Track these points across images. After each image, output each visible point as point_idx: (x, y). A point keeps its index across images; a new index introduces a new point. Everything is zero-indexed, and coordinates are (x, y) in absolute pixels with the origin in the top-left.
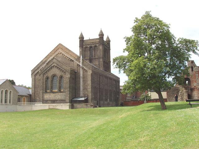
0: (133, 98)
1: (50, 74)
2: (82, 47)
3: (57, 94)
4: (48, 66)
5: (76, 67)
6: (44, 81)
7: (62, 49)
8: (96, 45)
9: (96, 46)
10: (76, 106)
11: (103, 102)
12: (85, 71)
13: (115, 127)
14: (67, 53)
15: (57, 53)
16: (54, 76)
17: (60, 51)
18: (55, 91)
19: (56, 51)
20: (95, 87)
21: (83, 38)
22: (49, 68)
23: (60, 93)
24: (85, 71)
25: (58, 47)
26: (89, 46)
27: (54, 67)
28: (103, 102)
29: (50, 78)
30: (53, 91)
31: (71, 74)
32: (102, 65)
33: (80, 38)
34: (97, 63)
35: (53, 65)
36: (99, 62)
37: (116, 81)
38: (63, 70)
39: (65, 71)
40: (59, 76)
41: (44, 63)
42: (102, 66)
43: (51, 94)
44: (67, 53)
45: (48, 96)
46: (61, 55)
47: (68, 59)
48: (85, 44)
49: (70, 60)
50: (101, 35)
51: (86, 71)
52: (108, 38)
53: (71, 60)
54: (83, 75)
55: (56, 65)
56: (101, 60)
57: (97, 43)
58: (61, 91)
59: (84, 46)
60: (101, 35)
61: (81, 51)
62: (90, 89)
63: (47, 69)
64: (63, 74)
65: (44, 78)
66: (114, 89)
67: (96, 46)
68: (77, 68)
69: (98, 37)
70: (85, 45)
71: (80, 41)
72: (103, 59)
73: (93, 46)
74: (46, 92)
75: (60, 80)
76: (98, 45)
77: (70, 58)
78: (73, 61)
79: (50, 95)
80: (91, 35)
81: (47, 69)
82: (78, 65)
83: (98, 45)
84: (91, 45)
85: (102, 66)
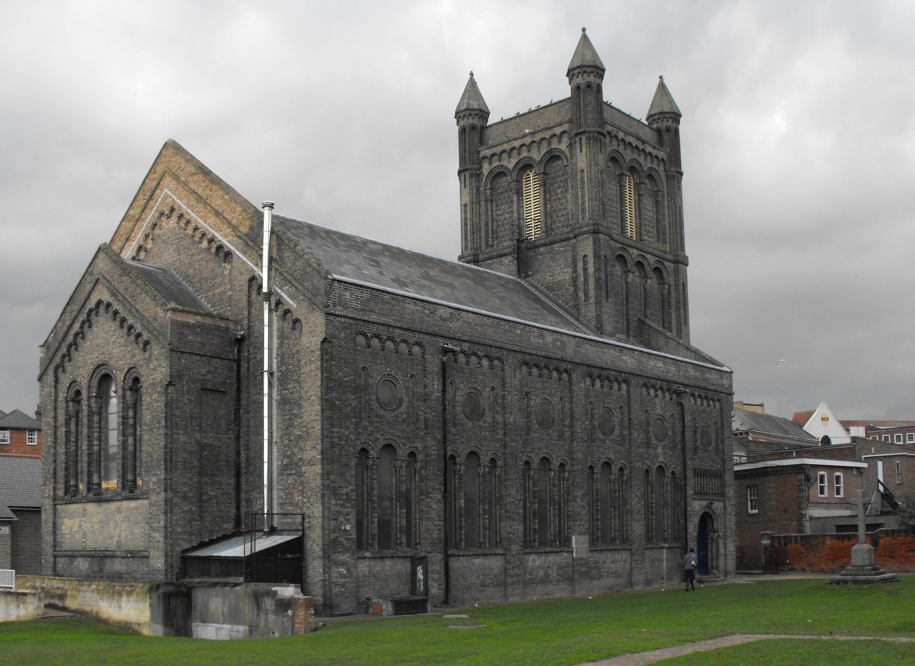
2: (478, 175)
4: (76, 307)
6: (61, 418)
8: (555, 145)
9: (553, 157)
10: (206, 606)
11: (721, 504)
15: (151, 216)
21: (484, 114)
23: (125, 504)
24: (288, 325)
25: (160, 169)
27: (102, 309)
28: (721, 504)
31: (175, 351)
33: (460, 115)
34: (562, 274)
35: (92, 303)
39: (146, 336)
42: (592, 293)
44: (200, 199)
48: (488, 153)
50: (587, 72)
53: (220, 248)
54: (282, 359)
59: (486, 168)
60: (587, 72)
61: (467, 199)
62: (318, 468)
67: (553, 157)
69: (564, 90)
72: (596, 242)
73: (536, 155)
76: (563, 146)
78: (228, 255)
80: (524, 82)
83: (563, 146)
84: (525, 154)
85: (592, 293)
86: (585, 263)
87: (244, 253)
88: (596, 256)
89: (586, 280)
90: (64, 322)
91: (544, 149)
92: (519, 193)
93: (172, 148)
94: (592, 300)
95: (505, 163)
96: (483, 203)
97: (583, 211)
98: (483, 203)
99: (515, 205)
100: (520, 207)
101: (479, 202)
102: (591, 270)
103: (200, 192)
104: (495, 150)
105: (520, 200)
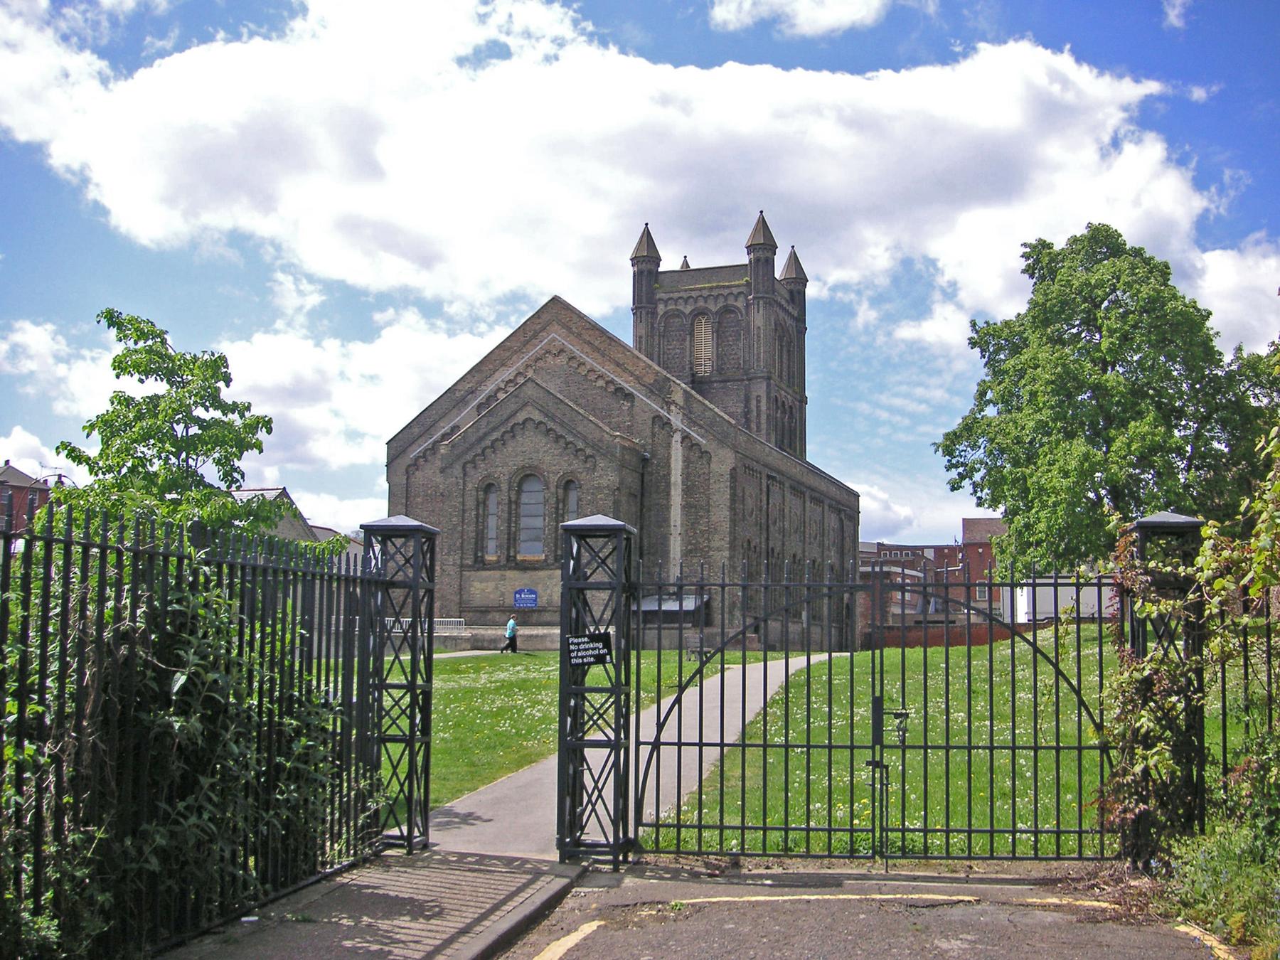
0: (925, 611)
1: (504, 465)
2: (653, 313)
3: (542, 574)
5: (648, 433)
6: (470, 503)
7: (569, 329)
8: (731, 301)
9: (727, 310)
12: (694, 455)
13: (1122, 644)
14: (597, 350)
16: (527, 475)
17: (554, 340)
18: (529, 557)
19: (535, 336)
20: (749, 542)
22: (496, 435)
24: (694, 455)
26: (688, 309)
27: (529, 425)
29: (504, 487)
30: (519, 557)
32: (764, 417)
33: (635, 260)
35: (521, 417)
36: (747, 400)
37: (840, 511)
38: (580, 445)
39: (589, 451)
40: (554, 479)
41: (463, 402)
42: (764, 426)
43: (509, 574)
45: (491, 585)
46: (562, 360)
47: (601, 383)
49: (611, 388)
50: (763, 245)
51: (705, 454)
52: (794, 259)
53: (620, 390)
54: (686, 476)
55: (537, 416)
56: (760, 389)
57: (735, 291)
58: (483, 561)
59: (661, 309)
61: (643, 332)
62: (726, 554)
63: (486, 435)
64: (577, 465)
65: (470, 486)
66: (832, 558)
67: (727, 310)
68: (653, 435)
70: (666, 302)
71: (638, 278)
72: (768, 386)
74: (480, 564)
75: (558, 502)
76: (740, 304)
77: (612, 382)
78: (629, 396)
79: (503, 578)
81: (486, 435)
82: (657, 418)
84: (701, 303)
85: (764, 426)
86: (759, 401)
87: (649, 398)
88: (768, 398)
89: (758, 415)
90: (478, 430)
91: (721, 303)
92: (692, 334)
93: (556, 300)
94: (764, 432)
95: (681, 308)
96: (656, 338)
97: (758, 360)
98: (656, 338)
99: (688, 343)
100: (692, 346)
101: (652, 337)
102: (763, 407)
103: (597, 343)
104: (682, 294)
105: (692, 341)
